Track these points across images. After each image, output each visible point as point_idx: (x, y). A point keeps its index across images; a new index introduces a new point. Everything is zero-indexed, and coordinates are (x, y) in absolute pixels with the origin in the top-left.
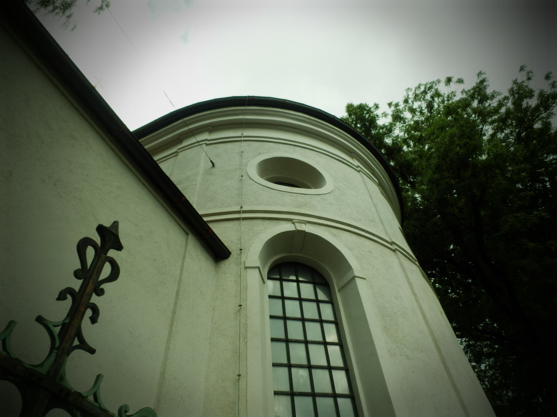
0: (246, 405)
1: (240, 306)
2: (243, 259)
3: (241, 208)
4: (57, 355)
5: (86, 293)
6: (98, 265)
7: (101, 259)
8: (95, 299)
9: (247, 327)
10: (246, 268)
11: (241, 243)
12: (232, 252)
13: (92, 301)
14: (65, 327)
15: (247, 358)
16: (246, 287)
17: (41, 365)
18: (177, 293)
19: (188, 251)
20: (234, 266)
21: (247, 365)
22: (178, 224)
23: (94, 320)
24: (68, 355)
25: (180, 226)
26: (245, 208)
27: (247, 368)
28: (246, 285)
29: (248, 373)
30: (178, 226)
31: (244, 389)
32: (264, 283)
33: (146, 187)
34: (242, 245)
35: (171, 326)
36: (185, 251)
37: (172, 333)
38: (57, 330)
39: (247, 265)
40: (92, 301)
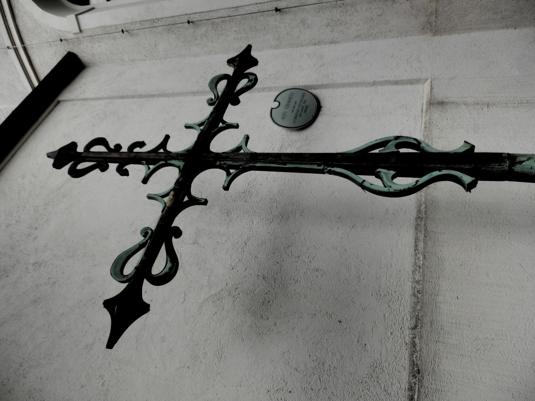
0: (213, 11)
1: (123, 31)
2: (71, 36)
3: (10, 48)
4: (171, 159)
5: (119, 157)
6: (93, 156)
7: (87, 155)
8: (124, 149)
9: (143, 21)
10: (81, 31)
11: (54, 42)
12: (68, 51)
13: (126, 151)
14: (149, 162)
15: (172, 17)
16: (102, 29)
17: (179, 167)
18: (122, 98)
19: (77, 97)
20: (82, 46)
21: (178, 16)
22: (49, 113)
23: (142, 144)
24: (171, 152)
25: (51, 111)
26: (9, 43)
27: (181, 15)
28: (100, 28)
29: (185, 14)
30: (52, 113)
31: (200, 15)
32: (93, 8)
33: (15, 154)
34: (56, 40)
35: (153, 96)
36: (78, 100)
37: (159, 94)
38: (152, 167)
39: (77, 30)
40: (126, 151)
